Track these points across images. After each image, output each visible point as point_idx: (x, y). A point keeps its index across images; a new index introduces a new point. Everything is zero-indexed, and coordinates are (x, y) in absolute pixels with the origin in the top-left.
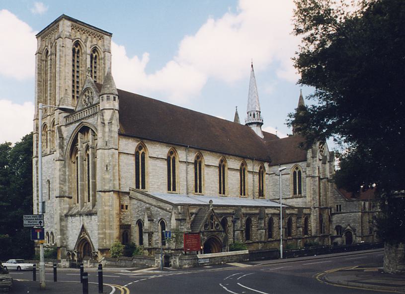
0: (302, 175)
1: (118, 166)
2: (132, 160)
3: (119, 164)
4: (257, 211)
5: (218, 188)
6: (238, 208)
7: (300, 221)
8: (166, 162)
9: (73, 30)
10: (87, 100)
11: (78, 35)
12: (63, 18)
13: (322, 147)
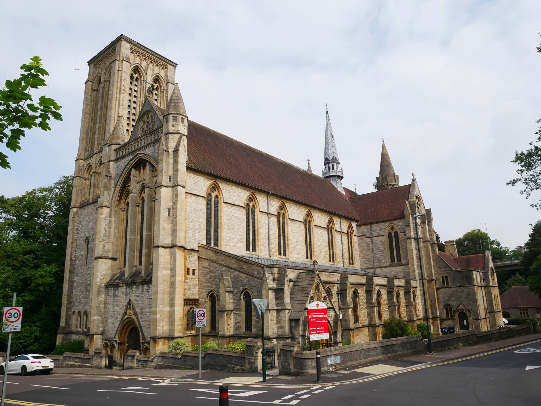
0: (399, 237)
1: (184, 210)
2: (202, 204)
3: (185, 208)
8: (244, 211)
10: (145, 127)
11: (138, 60)
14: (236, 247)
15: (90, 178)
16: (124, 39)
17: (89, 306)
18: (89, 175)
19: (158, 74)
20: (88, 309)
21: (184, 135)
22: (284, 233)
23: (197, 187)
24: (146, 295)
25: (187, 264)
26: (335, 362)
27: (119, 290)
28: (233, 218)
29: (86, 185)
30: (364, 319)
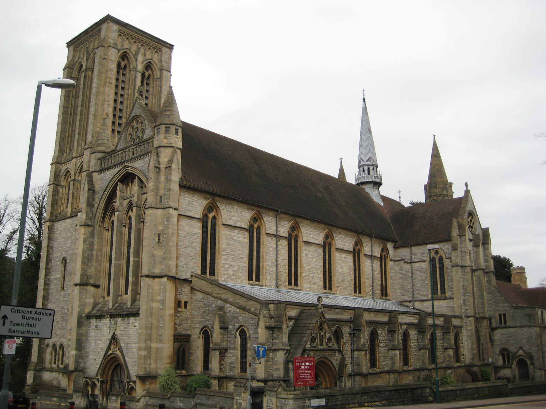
1: (176, 235)
2: (197, 228)
3: (178, 233)
4: (385, 319)
5: (323, 279)
6: (358, 312)
7: (447, 337)
8: (246, 234)
9: (120, 37)
12: (108, 19)
13: (471, 221)
14: (236, 276)
15: (67, 186)
16: (111, 20)
17: (66, 338)
18: (67, 182)
19: (151, 59)
20: (64, 342)
21: (178, 148)
22: (296, 259)
23: (191, 208)
24: (133, 329)
25: (178, 296)
26: (319, 404)
27: (102, 321)
28: (233, 242)
29: (63, 194)
30: (384, 363)
